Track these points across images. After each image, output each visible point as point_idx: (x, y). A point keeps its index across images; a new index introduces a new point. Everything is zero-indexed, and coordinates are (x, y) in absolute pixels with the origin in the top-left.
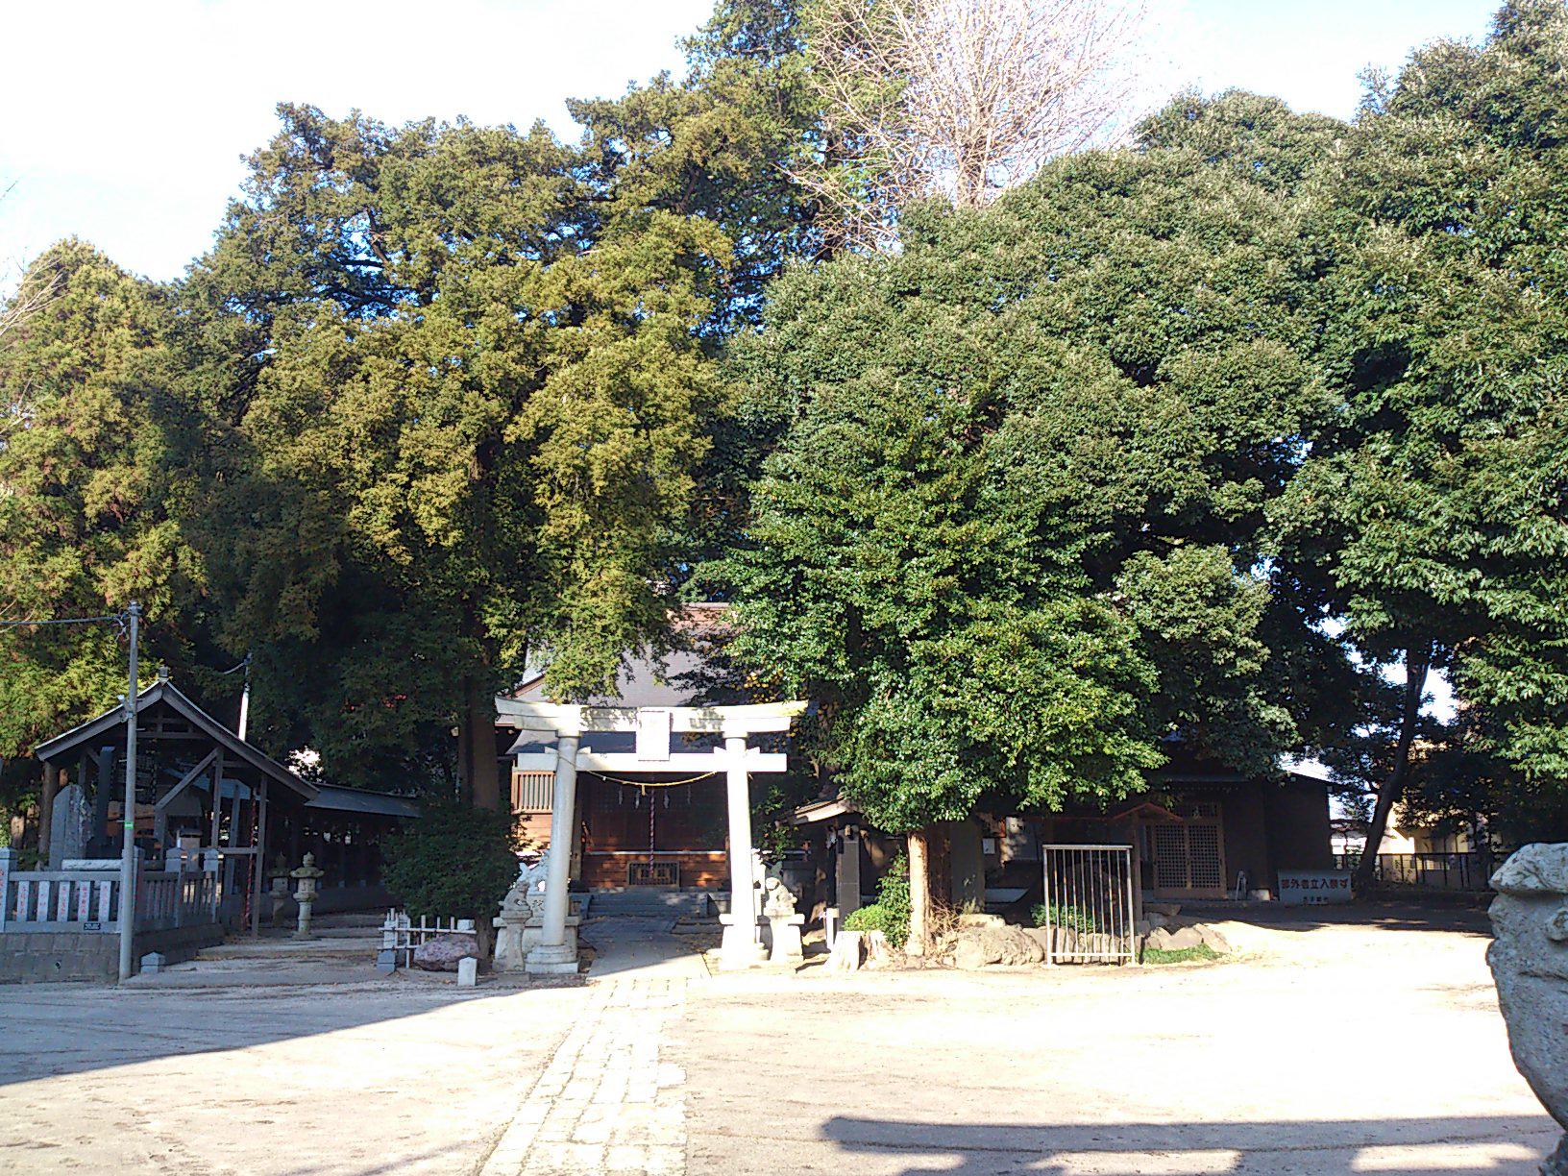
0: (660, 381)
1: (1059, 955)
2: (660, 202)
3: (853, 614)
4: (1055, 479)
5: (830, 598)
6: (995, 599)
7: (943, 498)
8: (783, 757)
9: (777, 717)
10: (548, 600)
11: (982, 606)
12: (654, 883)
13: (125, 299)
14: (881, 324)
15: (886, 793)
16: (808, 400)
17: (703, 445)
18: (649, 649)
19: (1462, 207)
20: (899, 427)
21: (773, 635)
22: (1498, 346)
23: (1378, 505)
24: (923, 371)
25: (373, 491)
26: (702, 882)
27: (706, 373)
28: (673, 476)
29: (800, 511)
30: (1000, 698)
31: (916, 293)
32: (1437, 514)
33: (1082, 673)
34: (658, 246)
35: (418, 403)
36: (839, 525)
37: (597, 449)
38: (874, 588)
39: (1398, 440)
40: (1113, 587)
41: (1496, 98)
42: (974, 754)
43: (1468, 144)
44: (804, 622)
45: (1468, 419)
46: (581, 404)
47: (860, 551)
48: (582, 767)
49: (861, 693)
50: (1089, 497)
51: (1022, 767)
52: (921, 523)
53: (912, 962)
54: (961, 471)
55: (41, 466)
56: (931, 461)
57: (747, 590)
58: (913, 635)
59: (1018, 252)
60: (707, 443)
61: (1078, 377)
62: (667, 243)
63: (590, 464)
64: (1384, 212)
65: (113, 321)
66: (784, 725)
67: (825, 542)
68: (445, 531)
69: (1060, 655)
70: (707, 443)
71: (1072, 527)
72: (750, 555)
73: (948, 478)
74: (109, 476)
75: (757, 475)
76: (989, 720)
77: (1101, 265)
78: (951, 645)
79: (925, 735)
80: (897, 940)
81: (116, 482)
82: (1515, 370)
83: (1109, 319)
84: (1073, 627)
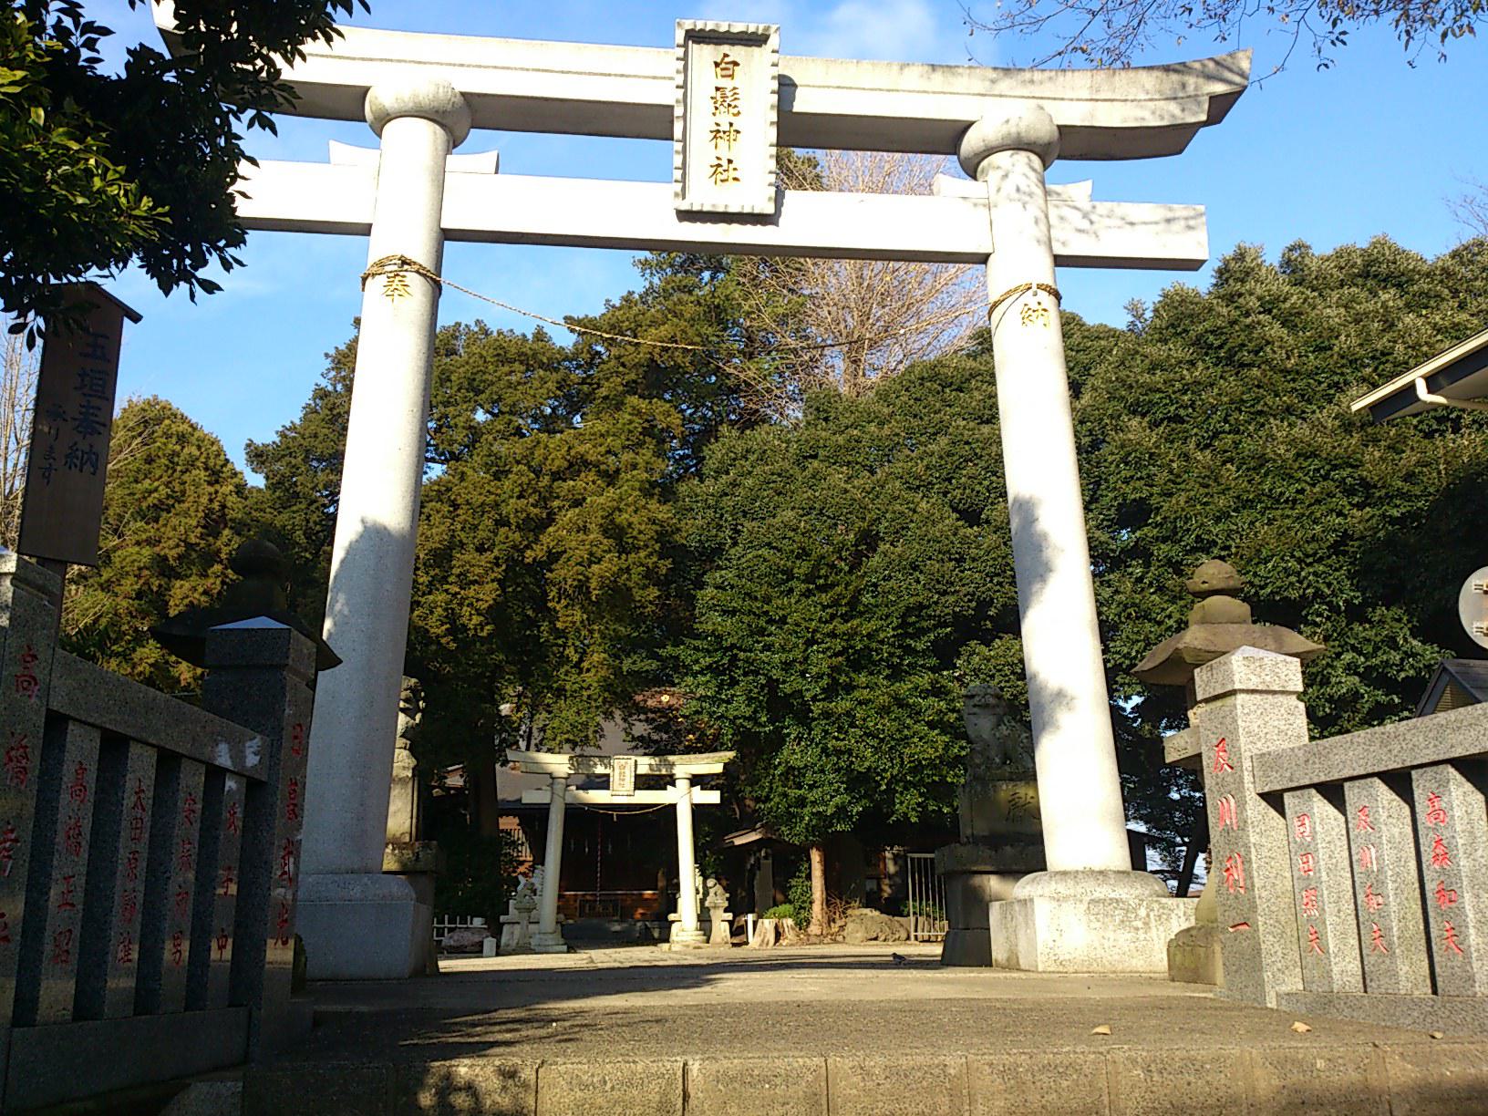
0: (635, 520)
1: (919, 933)
2: (631, 388)
3: (772, 684)
4: (912, 590)
5: (756, 673)
6: (871, 674)
7: (835, 603)
8: (718, 793)
9: (711, 764)
10: (547, 676)
11: (862, 679)
12: (599, 915)
13: (199, 448)
14: (791, 478)
15: (794, 816)
16: (738, 532)
17: (665, 566)
18: (618, 714)
19: (1186, 408)
20: (804, 554)
21: (715, 700)
22: (1206, 504)
23: (1131, 610)
24: (821, 513)
25: (431, 597)
26: (638, 916)
27: (663, 512)
28: (644, 587)
29: (733, 612)
30: (875, 742)
31: (815, 457)
32: (1170, 617)
33: (931, 725)
34: (631, 422)
35: (463, 535)
36: (762, 623)
37: (595, 568)
38: (787, 666)
39: (1147, 565)
40: (954, 667)
41: (1212, 332)
42: (858, 782)
43: (1192, 363)
44: (738, 690)
45: (1188, 553)
46: (581, 536)
47: (777, 641)
48: (569, 800)
49: (778, 741)
50: (936, 603)
51: (890, 791)
52: (820, 620)
53: (813, 939)
54: (847, 584)
55: (138, 577)
56: (826, 577)
57: (696, 668)
58: (814, 699)
59: (886, 431)
60: (668, 563)
61: (929, 520)
62: (637, 420)
63: (588, 579)
64: (1133, 410)
65: (192, 463)
66: (718, 768)
67: (752, 634)
68: (482, 626)
69: (916, 713)
70: (668, 563)
71: (925, 624)
72: (697, 643)
73: (838, 589)
74: (187, 585)
75: (701, 585)
76: (867, 758)
77: (943, 441)
78: (841, 705)
79: (822, 771)
80: (802, 924)
81: (194, 589)
82: (1218, 520)
83: (949, 480)
84: (926, 694)
